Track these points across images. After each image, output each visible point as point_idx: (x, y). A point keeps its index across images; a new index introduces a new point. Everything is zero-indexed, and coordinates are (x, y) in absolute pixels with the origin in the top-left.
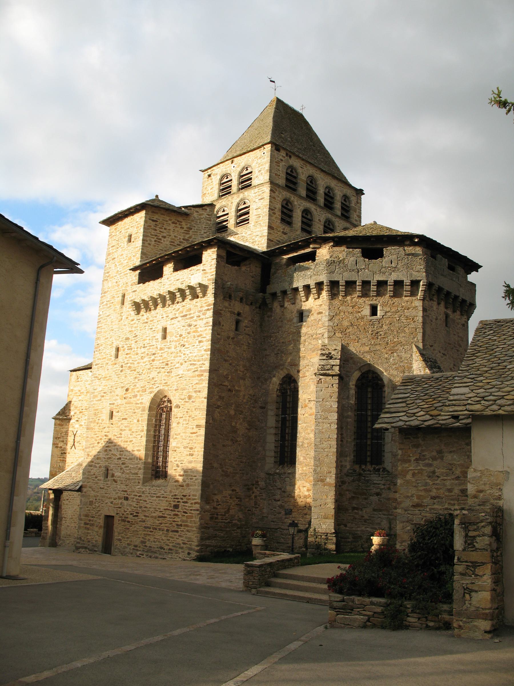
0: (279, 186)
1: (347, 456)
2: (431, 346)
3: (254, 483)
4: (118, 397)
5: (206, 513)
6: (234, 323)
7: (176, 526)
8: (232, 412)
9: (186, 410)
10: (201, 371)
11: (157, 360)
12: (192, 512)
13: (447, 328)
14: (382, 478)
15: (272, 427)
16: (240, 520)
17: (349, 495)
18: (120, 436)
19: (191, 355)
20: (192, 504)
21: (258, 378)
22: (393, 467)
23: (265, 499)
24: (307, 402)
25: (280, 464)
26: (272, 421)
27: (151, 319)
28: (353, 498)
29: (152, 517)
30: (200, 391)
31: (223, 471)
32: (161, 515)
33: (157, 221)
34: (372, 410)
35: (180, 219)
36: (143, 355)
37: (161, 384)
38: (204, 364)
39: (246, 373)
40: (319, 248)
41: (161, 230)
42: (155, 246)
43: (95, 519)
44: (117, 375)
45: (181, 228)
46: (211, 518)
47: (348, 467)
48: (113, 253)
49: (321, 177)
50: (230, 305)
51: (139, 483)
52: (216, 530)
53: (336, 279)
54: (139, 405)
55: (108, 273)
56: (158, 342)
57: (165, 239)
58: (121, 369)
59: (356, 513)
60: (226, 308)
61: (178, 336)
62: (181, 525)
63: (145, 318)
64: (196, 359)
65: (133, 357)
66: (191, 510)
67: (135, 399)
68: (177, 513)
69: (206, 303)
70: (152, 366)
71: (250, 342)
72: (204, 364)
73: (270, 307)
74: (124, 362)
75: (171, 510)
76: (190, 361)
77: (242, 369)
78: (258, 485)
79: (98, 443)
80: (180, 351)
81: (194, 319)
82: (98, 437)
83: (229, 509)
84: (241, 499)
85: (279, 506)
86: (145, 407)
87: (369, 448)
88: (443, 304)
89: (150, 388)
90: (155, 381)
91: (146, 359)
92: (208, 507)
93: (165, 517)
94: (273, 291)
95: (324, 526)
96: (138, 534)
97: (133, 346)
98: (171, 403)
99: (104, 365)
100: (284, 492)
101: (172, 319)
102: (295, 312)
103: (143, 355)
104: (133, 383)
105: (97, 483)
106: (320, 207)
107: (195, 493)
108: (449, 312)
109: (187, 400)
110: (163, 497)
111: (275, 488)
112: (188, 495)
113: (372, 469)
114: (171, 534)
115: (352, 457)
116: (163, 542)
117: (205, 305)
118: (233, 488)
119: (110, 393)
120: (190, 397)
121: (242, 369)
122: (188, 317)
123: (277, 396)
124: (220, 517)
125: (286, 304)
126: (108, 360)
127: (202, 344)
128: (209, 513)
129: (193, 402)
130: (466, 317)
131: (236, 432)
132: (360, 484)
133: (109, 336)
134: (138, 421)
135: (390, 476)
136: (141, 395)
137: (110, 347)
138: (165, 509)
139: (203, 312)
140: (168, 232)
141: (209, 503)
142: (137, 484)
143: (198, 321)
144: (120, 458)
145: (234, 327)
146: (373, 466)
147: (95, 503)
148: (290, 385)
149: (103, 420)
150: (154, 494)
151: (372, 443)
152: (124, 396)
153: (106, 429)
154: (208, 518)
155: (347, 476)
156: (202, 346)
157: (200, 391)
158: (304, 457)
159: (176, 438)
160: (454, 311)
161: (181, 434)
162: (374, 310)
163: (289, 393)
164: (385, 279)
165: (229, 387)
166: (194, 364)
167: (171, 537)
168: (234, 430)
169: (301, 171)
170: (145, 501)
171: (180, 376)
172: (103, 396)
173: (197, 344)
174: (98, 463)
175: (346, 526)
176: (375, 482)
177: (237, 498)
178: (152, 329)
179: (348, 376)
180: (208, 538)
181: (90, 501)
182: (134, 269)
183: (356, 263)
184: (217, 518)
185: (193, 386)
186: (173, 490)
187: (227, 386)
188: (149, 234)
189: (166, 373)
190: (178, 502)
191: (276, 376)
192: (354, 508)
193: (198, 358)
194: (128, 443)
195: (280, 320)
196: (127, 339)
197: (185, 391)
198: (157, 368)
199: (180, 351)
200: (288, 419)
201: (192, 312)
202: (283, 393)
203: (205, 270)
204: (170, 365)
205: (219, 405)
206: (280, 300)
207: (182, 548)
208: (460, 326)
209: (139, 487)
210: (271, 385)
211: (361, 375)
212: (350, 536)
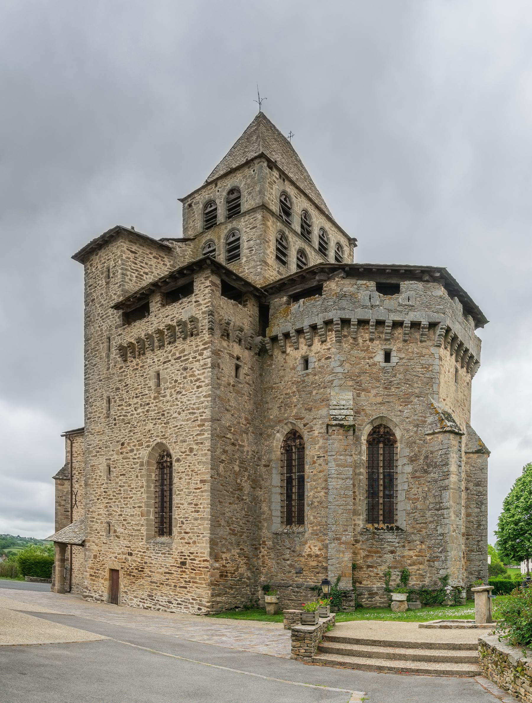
0: (274, 213)
1: (360, 515)
2: (444, 400)
3: (261, 542)
4: (114, 452)
5: (216, 571)
6: (234, 368)
7: (184, 583)
8: (237, 469)
9: (188, 464)
10: (202, 420)
11: (152, 411)
12: (201, 569)
13: (456, 384)
14: (396, 536)
15: (278, 486)
16: (249, 578)
17: (363, 554)
18: (119, 492)
19: (189, 402)
20: (199, 561)
21: (261, 434)
23: (273, 559)
24: (316, 458)
25: (287, 525)
26: (276, 480)
27: (141, 365)
28: (367, 556)
29: (158, 573)
30: (202, 443)
31: (230, 529)
32: (167, 571)
33: (136, 253)
34: (384, 467)
35: (162, 254)
36: (136, 406)
37: (158, 436)
38: (205, 413)
39: (248, 428)
40: (326, 281)
41: (142, 264)
42: (137, 283)
43: (100, 572)
44: (111, 429)
45: (164, 264)
46: (221, 576)
47: (362, 526)
48: (91, 293)
49: (315, 215)
50: (228, 346)
51: (142, 539)
52: (226, 587)
53: (347, 317)
54: (137, 460)
55: (89, 317)
56: (151, 390)
57: (147, 276)
58: (114, 422)
59: (371, 571)
60: (225, 348)
61: (173, 381)
62: (189, 582)
63: (135, 364)
64: (194, 407)
65: (125, 408)
66: (200, 567)
67: (131, 454)
68: (184, 569)
69: (202, 341)
70: (148, 417)
71: (251, 392)
72: (205, 413)
73: (270, 353)
74: (117, 415)
75: (178, 567)
76: (189, 409)
77: (244, 423)
78: (265, 545)
79: (98, 499)
80: (176, 399)
81: (189, 361)
82: (96, 493)
83: (238, 568)
84: (248, 558)
85: (288, 565)
86: (143, 462)
87: (381, 507)
88: (454, 356)
89: (147, 442)
90: (152, 434)
91: (139, 411)
92: (217, 565)
93: (172, 573)
94: (274, 334)
96: (144, 589)
97: (124, 397)
98: (171, 458)
99: (96, 419)
100: (293, 551)
101: (164, 363)
102: (299, 358)
103: (136, 406)
104: (128, 437)
105: (100, 538)
106: (315, 249)
107: (203, 551)
108: (459, 367)
109: (188, 453)
110: (168, 554)
111: (284, 547)
112: (195, 552)
113: (385, 528)
114: (178, 589)
115: (365, 516)
116: (170, 596)
117: (202, 343)
118: (241, 547)
119: (106, 448)
120: (191, 450)
121: (244, 423)
122: (183, 358)
123: (282, 454)
124: (229, 575)
125: (289, 350)
126: (99, 413)
127: (200, 389)
128: (219, 571)
129: (195, 455)
130: (470, 376)
131: (242, 490)
132: (375, 543)
133: (98, 387)
134: (137, 477)
136: (138, 450)
137: (100, 399)
138: (171, 566)
139: (199, 352)
140: (150, 268)
141: (218, 561)
142: (140, 540)
143: (195, 363)
144: (121, 515)
145: (233, 373)
146: (386, 525)
147: (99, 557)
148: (295, 442)
149: (100, 476)
150: (159, 550)
151: (384, 501)
152: (120, 451)
153: (105, 486)
154: (218, 576)
155: (361, 534)
156: (201, 392)
157: (202, 443)
158: (313, 516)
159: (179, 494)
160: (462, 367)
161: (184, 490)
162: (387, 357)
163: (294, 450)
164: (401, 319)
165: (232, 440)
166: (194, 413)
167: (179, 593)
168: (240, 489)
169: (295, 202)
170: (150, 557)
171: (179, 427)
172: (98, 452)
173: (196, 389)
174: (99, 519)
175: (361, 583)
176: (389, 540)
177: (245, 557)
178: (143, 376)
179: (360, 430)
180: (219, 595)
181: (94, 555)
182: (117, 307)
183: (370, 299)
184: (226, 576)
185: (193, 437)
186: (179, 547)
187: (231, 439)
188: (129, 268)
189: (163, 425)
190: (185, 559)
191: (280, 431)
192: (369, 566)
193: (197, 406)
194: (128, 499)
195: (283, 368)
196: (118, 389)
197: (186, 444)
198: (152, 419)
199: (176, 399)
200: (294, 477)
201: (186, 353)
202: (287, 451)
203: (198, 301)
204: (166, 415)
205: (224, 459)
206: (282, 344)
207: (192, 603)
208: (465, 384)
209: (142, 543)
210: (275, 441)
211: (372, 429)
212: (366, 593)
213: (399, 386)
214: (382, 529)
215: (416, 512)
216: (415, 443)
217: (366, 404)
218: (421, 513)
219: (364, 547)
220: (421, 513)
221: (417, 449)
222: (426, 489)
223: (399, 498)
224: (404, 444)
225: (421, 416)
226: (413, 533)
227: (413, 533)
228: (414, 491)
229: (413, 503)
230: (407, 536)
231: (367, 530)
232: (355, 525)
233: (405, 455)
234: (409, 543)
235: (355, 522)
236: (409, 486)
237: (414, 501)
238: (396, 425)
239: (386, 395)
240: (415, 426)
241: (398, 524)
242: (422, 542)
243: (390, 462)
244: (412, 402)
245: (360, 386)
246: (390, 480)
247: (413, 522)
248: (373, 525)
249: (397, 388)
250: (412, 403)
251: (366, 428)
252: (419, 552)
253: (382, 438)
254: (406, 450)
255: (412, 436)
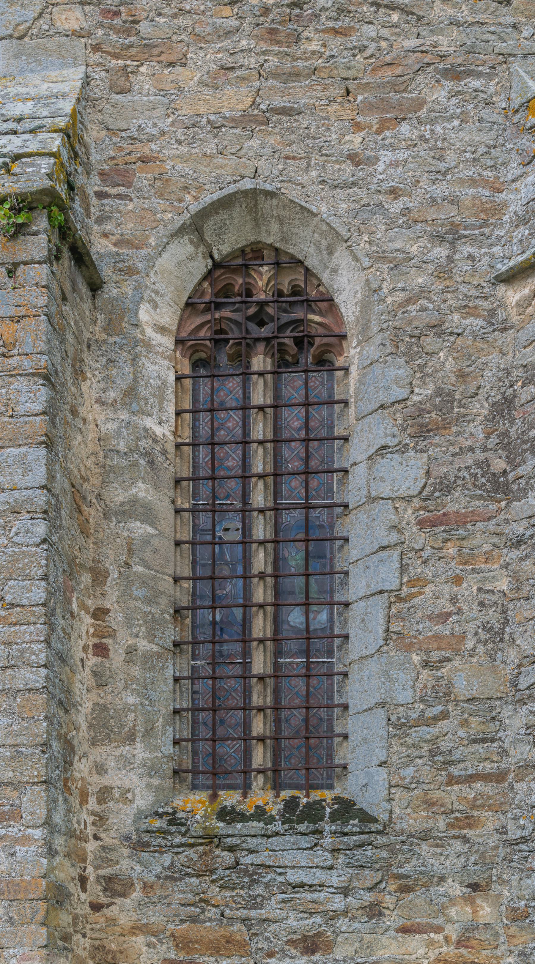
1: (131, 738)
22: (398, 792)
47: (143, 800)
95: (233, 483)
113: (275, 808)
135: (382, 840)
146: (286, 794)
155: (140, 846)
176: (293, 877)
179: (130, 271)
213: (346, 21)
214: (260, 814)
215: (445, 715)
216: (437, 329)
217: (165, 124)
218: (474, 721)
219: (155, 916)
220: (474, 721)
221: (450, 364)
222: (504, 585)
223: (357, 648)
224: (378, 339)
225: (473, 182)
226: (426, 836)
227: (426, 836)
228: (435, 595)
229: (426, 664)
230: (394, 852)
231: (173, 822)
232: (104, 795)
233: (383, 397)
234: (406, 889)
235: (105, 781)
236: (403, 568)
237: (435, 656)
238: (334, 239)
239: (276, 75)
240: (438, 238)
241: (349, 788)
242: (475, 887)
243: (311, 458)
244: (420, 103)
245: (128, 33)
246: (313, 543)
247: (427, 773)
248: (214, 797)
249: (336, 32)
250: (422, 113)
251: (166, 261)
252: (459, 944)
253: (259, 319)
254: (391, 372)
255: (424, 292)
